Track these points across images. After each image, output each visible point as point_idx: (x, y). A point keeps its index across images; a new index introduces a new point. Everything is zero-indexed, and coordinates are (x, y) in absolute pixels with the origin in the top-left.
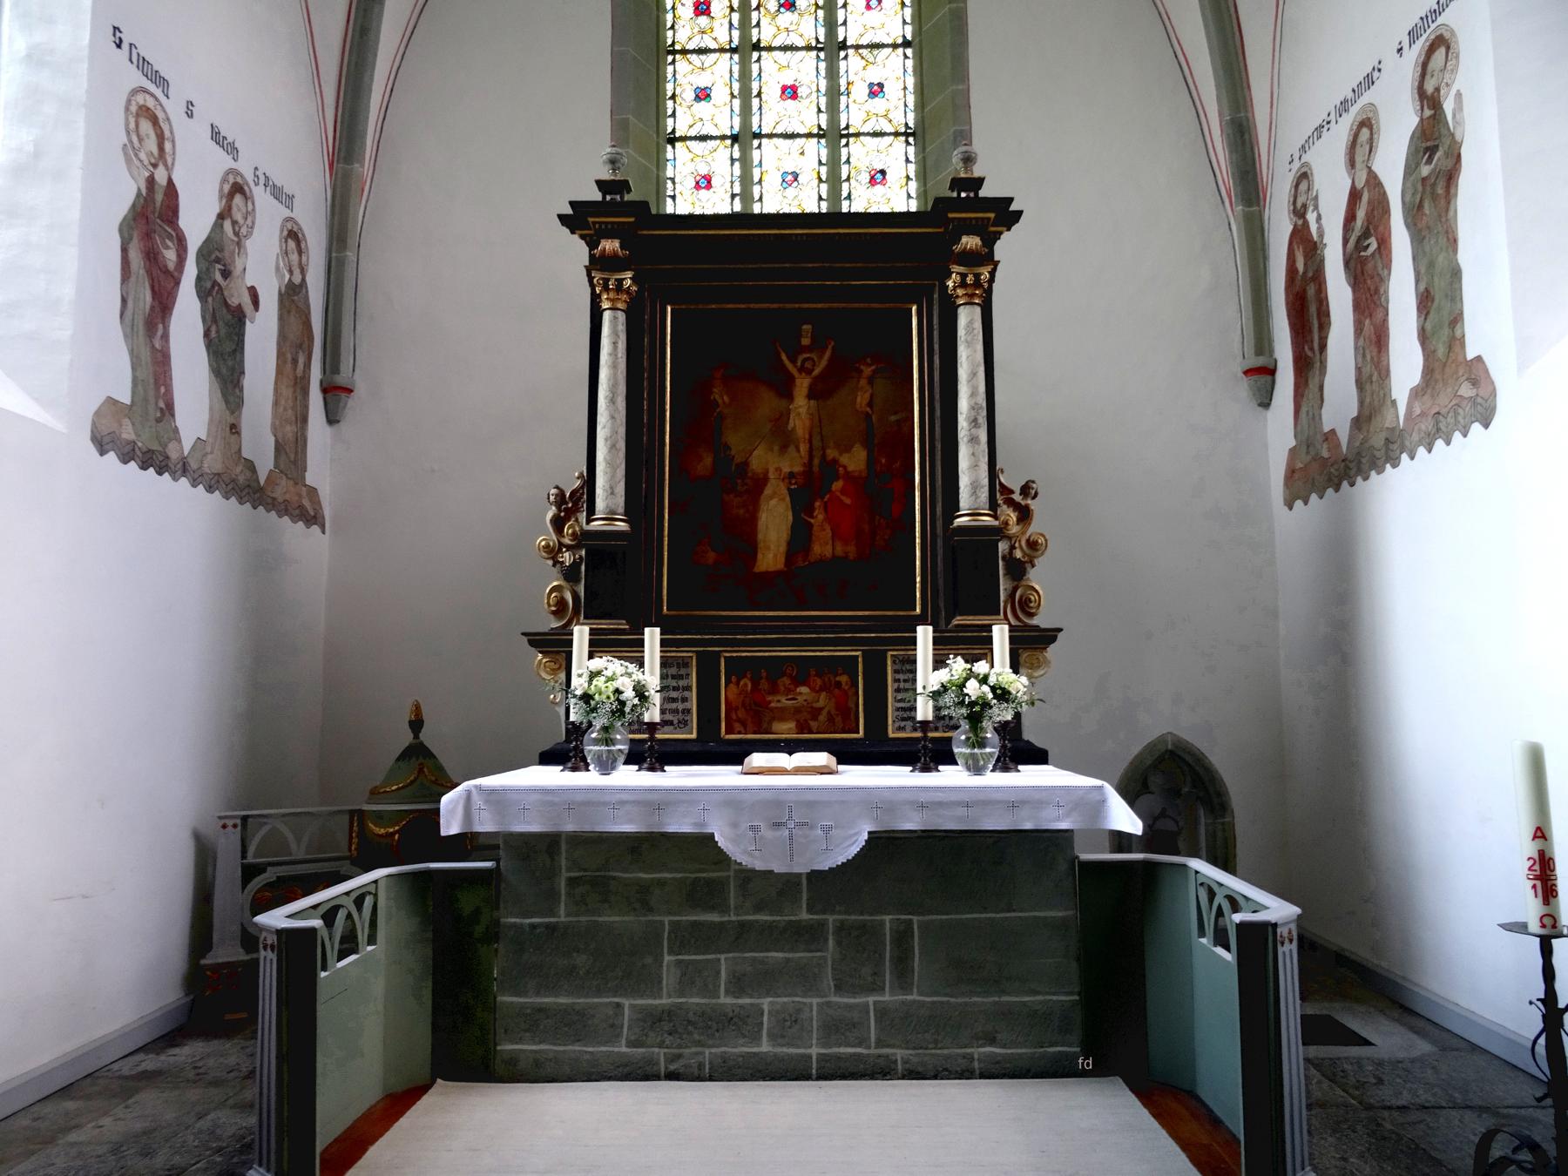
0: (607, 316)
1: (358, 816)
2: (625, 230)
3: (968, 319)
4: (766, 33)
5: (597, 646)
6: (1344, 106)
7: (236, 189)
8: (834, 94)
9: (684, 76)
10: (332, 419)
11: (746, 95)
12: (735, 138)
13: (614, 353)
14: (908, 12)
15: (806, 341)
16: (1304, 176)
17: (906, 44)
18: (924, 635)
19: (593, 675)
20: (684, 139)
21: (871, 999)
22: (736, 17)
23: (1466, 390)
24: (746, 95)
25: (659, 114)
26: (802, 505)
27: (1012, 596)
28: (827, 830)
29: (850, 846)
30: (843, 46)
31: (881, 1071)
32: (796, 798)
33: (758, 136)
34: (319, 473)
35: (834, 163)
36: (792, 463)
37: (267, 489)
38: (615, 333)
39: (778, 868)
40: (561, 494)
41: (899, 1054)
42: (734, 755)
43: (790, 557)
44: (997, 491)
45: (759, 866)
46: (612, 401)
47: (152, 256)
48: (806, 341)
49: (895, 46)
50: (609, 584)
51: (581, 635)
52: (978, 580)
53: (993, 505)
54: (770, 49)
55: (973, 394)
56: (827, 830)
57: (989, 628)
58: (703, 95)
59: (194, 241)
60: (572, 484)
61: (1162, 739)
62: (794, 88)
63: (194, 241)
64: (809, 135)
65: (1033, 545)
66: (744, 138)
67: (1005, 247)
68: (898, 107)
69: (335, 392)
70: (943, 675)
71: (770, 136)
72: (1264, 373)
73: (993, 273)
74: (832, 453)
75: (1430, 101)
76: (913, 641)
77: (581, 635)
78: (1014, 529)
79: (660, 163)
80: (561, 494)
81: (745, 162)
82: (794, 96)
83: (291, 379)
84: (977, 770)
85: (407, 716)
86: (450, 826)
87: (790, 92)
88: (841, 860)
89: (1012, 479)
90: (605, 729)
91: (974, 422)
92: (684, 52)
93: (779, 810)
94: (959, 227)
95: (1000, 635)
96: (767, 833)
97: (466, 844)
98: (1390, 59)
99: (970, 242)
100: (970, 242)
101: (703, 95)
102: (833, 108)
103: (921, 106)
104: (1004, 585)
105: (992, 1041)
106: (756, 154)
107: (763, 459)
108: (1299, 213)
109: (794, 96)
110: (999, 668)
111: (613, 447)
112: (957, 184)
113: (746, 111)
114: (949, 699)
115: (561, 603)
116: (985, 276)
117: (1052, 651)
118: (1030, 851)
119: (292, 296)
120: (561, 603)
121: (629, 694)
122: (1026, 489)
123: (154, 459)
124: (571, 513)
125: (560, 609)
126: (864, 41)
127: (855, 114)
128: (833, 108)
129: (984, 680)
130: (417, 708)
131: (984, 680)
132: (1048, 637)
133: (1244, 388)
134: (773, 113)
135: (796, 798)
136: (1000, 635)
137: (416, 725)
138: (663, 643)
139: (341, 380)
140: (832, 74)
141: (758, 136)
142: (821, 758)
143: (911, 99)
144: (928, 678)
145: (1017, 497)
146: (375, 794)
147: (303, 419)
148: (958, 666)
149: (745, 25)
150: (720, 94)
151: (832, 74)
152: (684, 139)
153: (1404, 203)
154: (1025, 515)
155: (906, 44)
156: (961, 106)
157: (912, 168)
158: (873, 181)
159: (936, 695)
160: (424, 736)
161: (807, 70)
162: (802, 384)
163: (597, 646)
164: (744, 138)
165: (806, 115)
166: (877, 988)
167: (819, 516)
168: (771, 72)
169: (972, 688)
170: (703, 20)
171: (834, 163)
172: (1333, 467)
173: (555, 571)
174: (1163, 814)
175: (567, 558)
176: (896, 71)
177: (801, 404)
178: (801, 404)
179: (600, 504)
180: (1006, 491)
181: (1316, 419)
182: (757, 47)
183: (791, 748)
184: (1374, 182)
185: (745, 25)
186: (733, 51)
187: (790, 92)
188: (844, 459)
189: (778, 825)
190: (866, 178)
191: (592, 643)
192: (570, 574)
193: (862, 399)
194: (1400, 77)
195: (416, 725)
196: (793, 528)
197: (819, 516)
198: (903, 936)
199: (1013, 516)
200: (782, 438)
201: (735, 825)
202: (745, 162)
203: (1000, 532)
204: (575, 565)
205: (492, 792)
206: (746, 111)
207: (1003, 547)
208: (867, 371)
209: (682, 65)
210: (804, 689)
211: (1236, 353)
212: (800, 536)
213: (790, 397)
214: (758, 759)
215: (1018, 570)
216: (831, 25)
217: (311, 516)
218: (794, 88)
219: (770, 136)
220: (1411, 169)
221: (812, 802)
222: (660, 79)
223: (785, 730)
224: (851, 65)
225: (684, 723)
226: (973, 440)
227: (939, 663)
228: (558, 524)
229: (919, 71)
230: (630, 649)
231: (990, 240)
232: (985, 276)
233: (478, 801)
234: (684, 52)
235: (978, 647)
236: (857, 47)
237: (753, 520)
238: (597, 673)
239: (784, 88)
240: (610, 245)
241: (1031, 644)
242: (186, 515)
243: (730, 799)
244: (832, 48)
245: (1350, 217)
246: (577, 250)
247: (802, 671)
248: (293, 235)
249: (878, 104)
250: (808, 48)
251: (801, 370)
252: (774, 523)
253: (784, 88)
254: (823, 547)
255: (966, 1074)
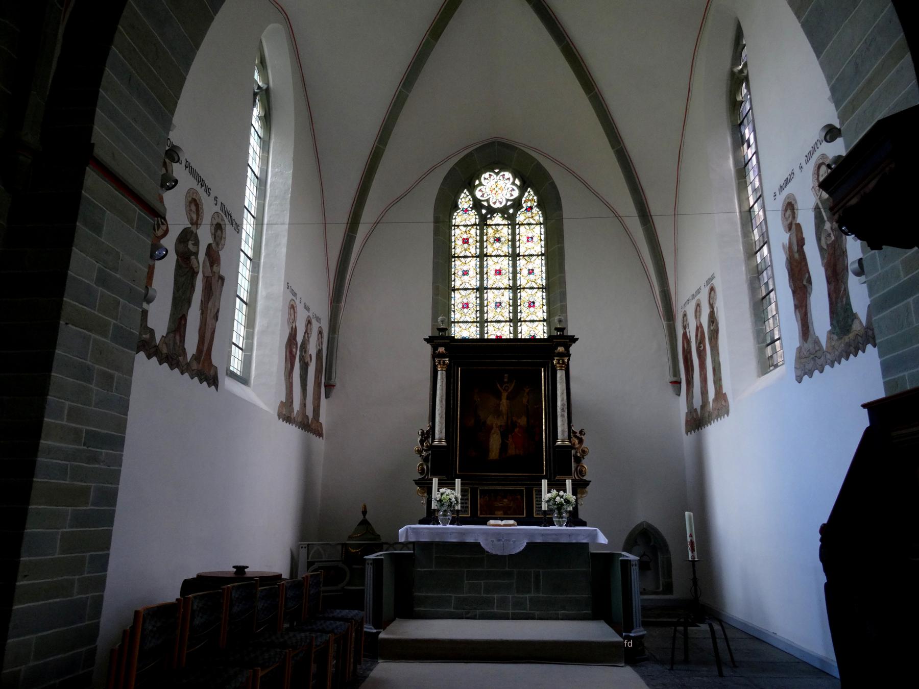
0: (439, 373)
1: (344, 545)
2: (442, 342)
3: (560, 374)
4: (489, 250)
5: (441, 485)
6: (694, 296)
7: (309, 322)
8: (515, 273)
9: (458, 266)
10: (327, 397)
11: (482, 273)
12: (477, 289)
13: (442, 385)
14: (543, 243)
15: (506, 380)
16: (685, 315)
17: (542, 255)
18: (544, 482)
19: (442, 494)
20: (458, 289)
21: (527, 596)
22: (478, 244)
23: (723, 403)
24: (482, 273)
25: (450, 281)
26: (504, 436)
27: (576, 469)
28: (514, 542)
29: (522, 546)
30: (518, 255)
31: (533, 618)
32: (503, 533)
33: (487, 288)
34: (323, 419)
35: (515, 299)
36: (501, 422)
37: (310, 426)
38: (442, 378)
39: (499, 553)
40: (423, 432)
41: (537, 613)
42: (484, 523)
43: (500, 453)
44: (571, 433)
45: (494, 553)
46: (441, 401)
47: (291, 352)
48: (506, 380)
49: (538, 255)
50: (439, 463)
51: (435, 481)
52: (565, 463)
53: (570, 438)
54: (491, 256)
55: (562, 400)
56: (514, 542)
57: (565, 480)
58: (465, 273)
59: (299, 343)
60: (426, 428)
61: (641, 524)
62: (500, 271)
63: (299, 343)
64: (505, 288)
65: (584, 451)
66: (481, 290)
67: (573, 349)
68: (539, 277)
69: (329, 387)
70: (549, 495)
71: (491, 289)
72: (677, 383)
73: (569, 360)
74: (514, 419)
75: (712, 306)
76: (541, 484)
77: (435, 481)
78: (577, 446)
79: (449, 298)
80: (423, 432)
81: (481, 298)
82: (500, 274)
83: (318, 384)
84: (561, 525)
85: (361, 510)
86: (402, 539)
87: (498, 272)
88: (518, 551)
89: (576, 428)
90: (445, 511)
91: (563, 410)
92: (459, 257)
93: (498, 536)
94: (558, 344)
95: (569, 483)
96: (496, 542)
97: (406, 545)
98: (703, 287)
99: (561, 349)
100: (561, 349)
101: (465, 273)
102: (515, 279)
103: (548, 278)
104: (574, 465)
105: (564, 609)
106: (485, 295)
107: (491, 420)
108: (685, 328)
109: (500, 274)
110: (569, 495)
111: (441, 417)
112: (557, 329)
113: (482, 280)
114: (551, 503)
115: (423, 469)
116: (566, 360)
117: (588, 488)
118: (577, 551)
119: (319, 352)
120: (423, 469)
121: (453, 500)
122: (581, 432)
123: (288, 419)
124: (427, 438)
125: (422, 471)
126: (526, 253)
127: (522, 281)
128: (515, 279)
129: (562, 497)
130: (365, 507)
131: (562, 497)
132: (587, 483)
133: (670, 389)
134: (492, 280)
135: (503, 533)
136: (569, 483)
137: (364, 512)
138: (462, 484)
139: (332, 382)
140: (514, 266)
141: (487, 288)
142: (512, 522)
143: (544, 275)
144: (546, 496)
145: (578, 435)
146: (350, 538)
147: (319, 398)
148: (554, 492)
149: (482, 247)
150: (472, 273)
151: (514, 266)
152: (458, 289)
153: (821, 249)
154: (581, 441)
155: (542, 255)
156: (562, 282)
157: (544, 301)
158: (530, 306)
159: (548, 502)
160: (367, 516)
161: (505, 264)
162: (505, 395)
163: (441, 485)
164: (481, 290)
165: (505, 281)
166: (529, 592)
167: (510, 440)
168: (491, 265)
169: (558, 499)
170: (466, 246)
171: (515, 299)
172: (697, 422)
173: (420, 459)
174: (644, 554)
175: (424, 454)
176: (538, 265)
177: (504, 401)
178: (504, 401)
179: (437, 436)
180: (574, 433)
181: (692, 403)
182: (486, 255)
183: (502, 519)
184: (701, 324)
185: (482, 247)
186: (477, 257)
187: (498, 272)
188: (519, 421)
189: (499, 540)
190: (527, 304)
191: (439, 484)
192: (426, 460)
193: (525, 400)
194: (704, 297)
195: (364, 512)
196: (502, 444)
197: (510, 440)
198: (537, 576)
199: (577, 441)
200: (498, 413)
201: (486, 540)
202: (481, 298)
203: (572, 447)
204: (428, 456)
205: (414, 529)
206: (482, 280)
207: (573, 452)
208: (527, 390)
209: (458, 262)
210: (505, 500)
211: (669, 378)
212: (504, 447)
213: (501, 400)
214: (492, 522)
215: (578, 460)
216: (514, 247)
217: (320, 434)
218: (500, 271)
219: (491, 289)
220: (709, 327)
221: (509, 534)
222: (450, 267)
223: (500, 513)
224: (522, 262)
225: (466, 511)
226: (562, 416)
227: (549, 492)
228: (422, 442)
229: (547, 265)
230: (452, 486)
231: (567, 348)
232: (566, 360)
233: (410, 532)
234: (459, 257)
235: (561, 487)
236: (524, 256)
237: (488, 441)
238: (438, 493)
239: (496, 271)
240: (441, 350)
241: (580, 486)
242: (292, 432)
243: (485, 533)
244: (514, 256)
245: (697, 335)
246: (428, 348)
247: (505, 494)
248: (320, 333)
249: (532, 277)
250: (505, 256)
251: (504, 390)
252: (495, 442)
253: (496, 271)
254: (512, 451)
255: (557, 619)
